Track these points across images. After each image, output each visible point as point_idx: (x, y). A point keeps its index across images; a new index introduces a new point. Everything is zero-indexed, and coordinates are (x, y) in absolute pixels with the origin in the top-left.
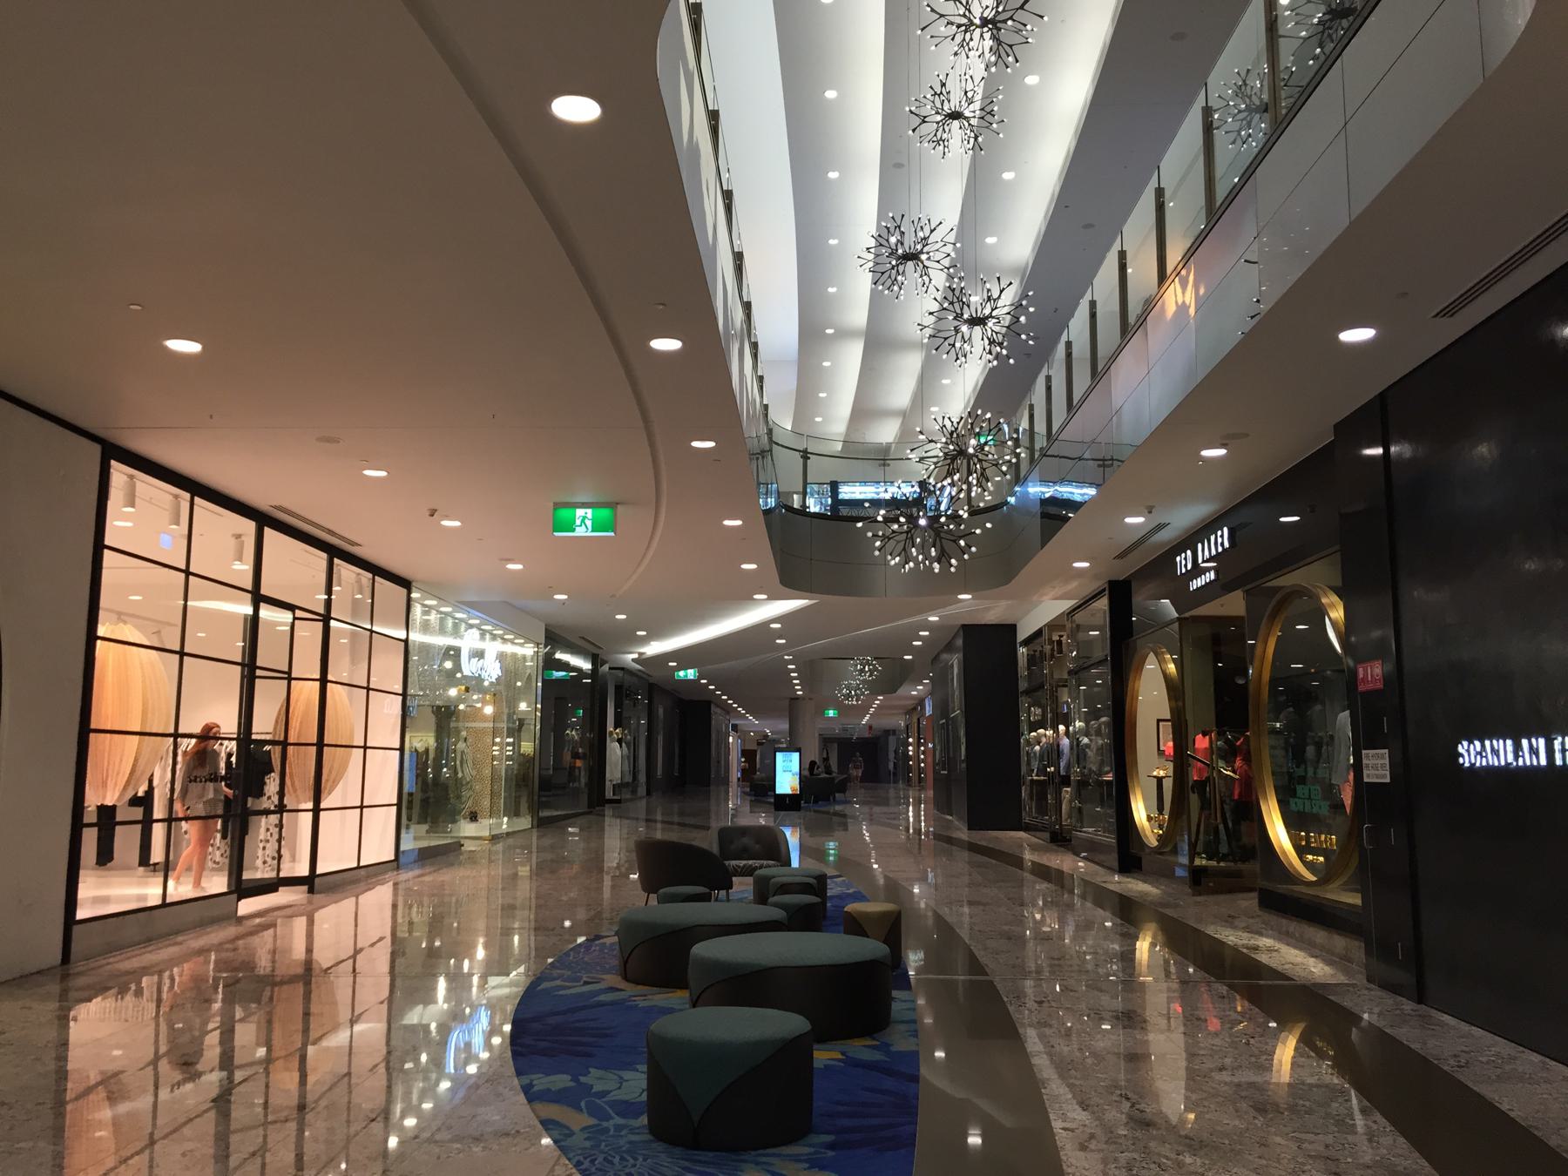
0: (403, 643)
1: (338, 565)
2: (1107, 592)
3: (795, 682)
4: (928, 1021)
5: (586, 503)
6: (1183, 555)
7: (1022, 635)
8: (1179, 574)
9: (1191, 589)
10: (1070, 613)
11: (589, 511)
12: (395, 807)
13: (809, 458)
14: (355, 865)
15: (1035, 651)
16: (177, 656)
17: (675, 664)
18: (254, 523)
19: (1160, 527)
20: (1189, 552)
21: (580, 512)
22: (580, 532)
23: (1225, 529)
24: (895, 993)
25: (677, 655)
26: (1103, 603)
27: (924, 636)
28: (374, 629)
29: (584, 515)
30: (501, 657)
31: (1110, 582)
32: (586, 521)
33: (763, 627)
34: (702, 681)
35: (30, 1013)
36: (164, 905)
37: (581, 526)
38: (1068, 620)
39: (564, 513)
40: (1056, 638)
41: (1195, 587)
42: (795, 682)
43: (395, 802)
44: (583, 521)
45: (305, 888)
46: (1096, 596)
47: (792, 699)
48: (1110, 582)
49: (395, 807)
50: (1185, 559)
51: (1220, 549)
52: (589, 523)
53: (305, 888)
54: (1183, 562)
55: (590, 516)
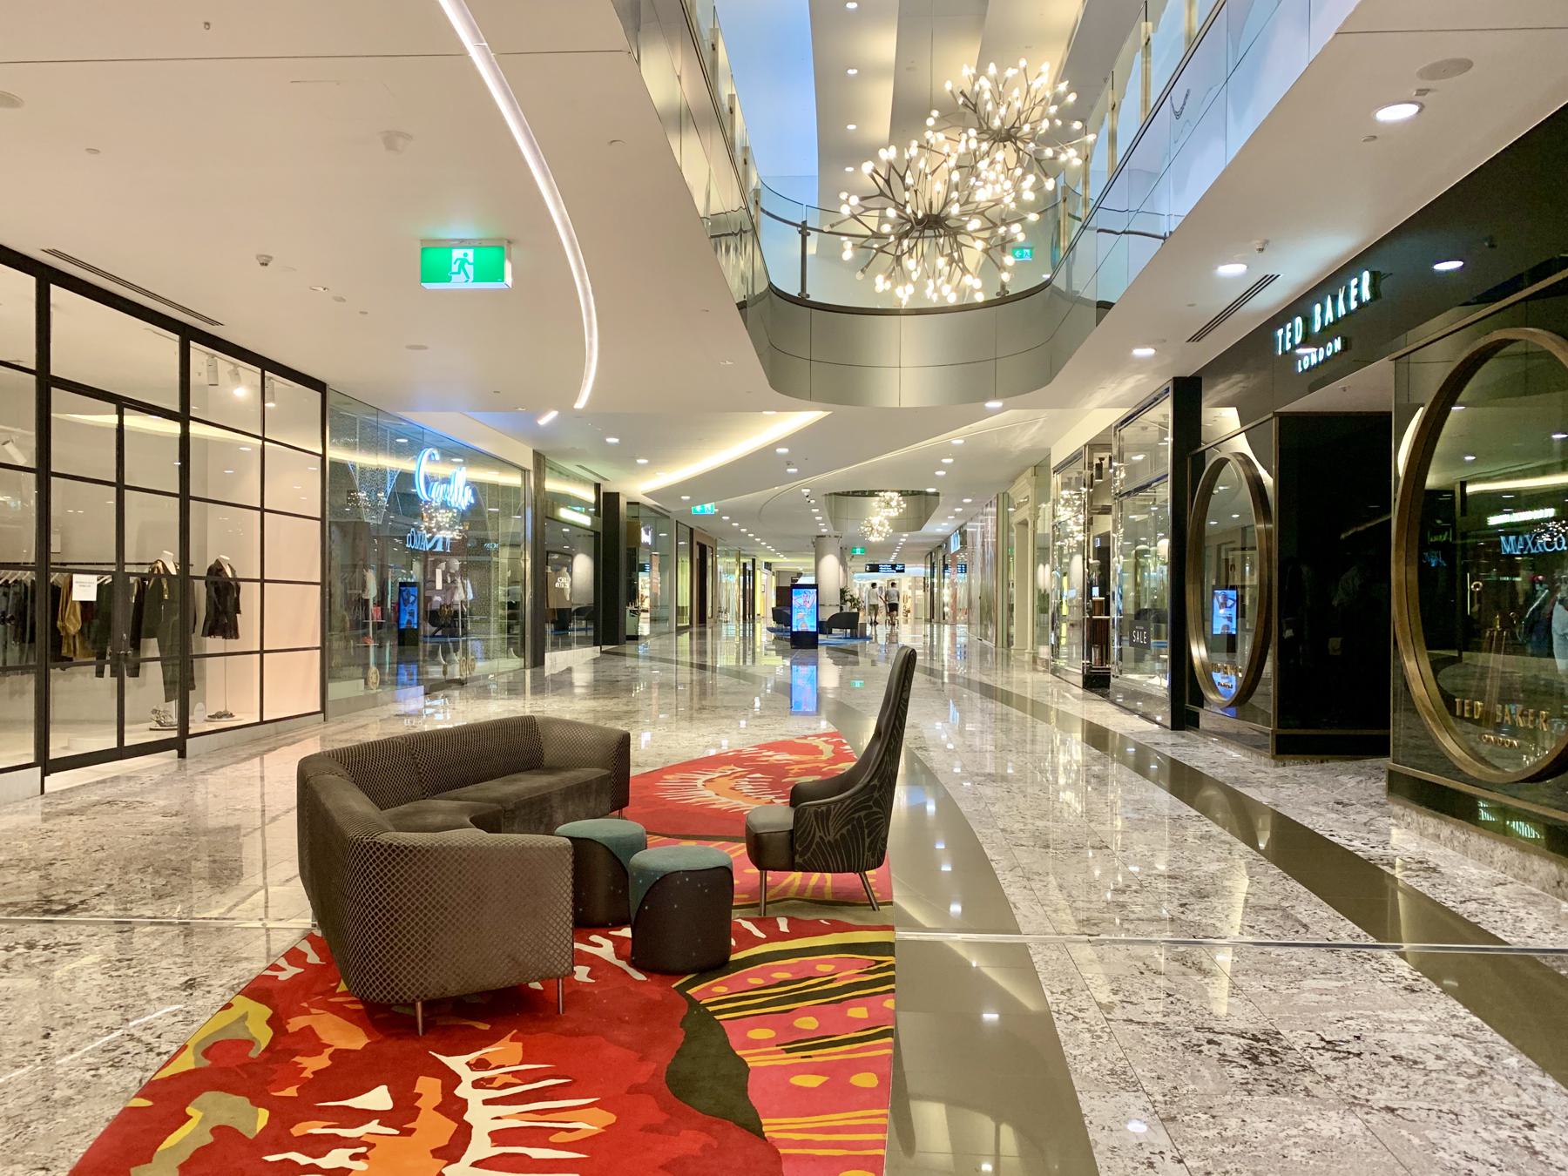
0: (319, 458)
1: (270, 378)
2: (1170, 393)
3: (818, 518)
4: (940, 846)
5: (462, 241)
6: (1289, 326)
7: (1054, 463)
8: (1280, 353)
9: (1300, 370)
10: (1116, 427)
11: (470, 252)
12: (319, 651)
13: (809, 234)
14: (258, 720)
15: (1070, 479)
16: (266, 507)
17: (688, 498)
18: (33, 279)
19: (1267, 280)
20: (1299, 321)
21: (457, 253)
22: (458, 283)
23: (1366, 275)
24: (764, 1121)
25: (690, 486)
26: (1166, 409)
27: (947, 464)
28: (260, 442)
29: (462, 256)
30: (470, 483)
31: (1176, 380)
32: (466, 265)
33: (767, 452)
34: (734, 524)
35: (1566, 458)
36: (262, 722)
37: (458, 273)
38: (1115, 434)
39: (434, 255)
40: (1096, 461)
41: (1306, 367)
42: (818, 518)
43: (318, 645)
44: (461, 267)
45: (175, 752)
46: (1154, 401)
47: (818, 537)
48: (1176, 380)
49: (319, 651)
50: (1292, 330)
51: (1354, 305)
52: (470, 269)
53: (175, 752)
54: (1289, 335)
55: (470, 258)
